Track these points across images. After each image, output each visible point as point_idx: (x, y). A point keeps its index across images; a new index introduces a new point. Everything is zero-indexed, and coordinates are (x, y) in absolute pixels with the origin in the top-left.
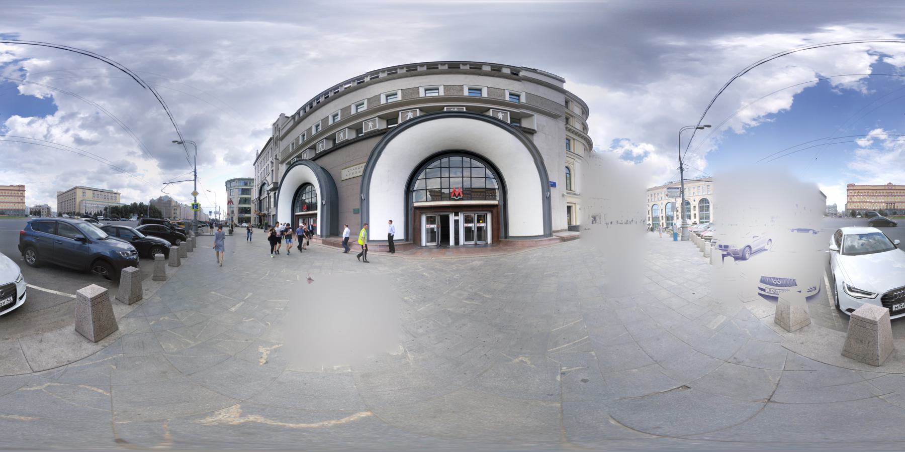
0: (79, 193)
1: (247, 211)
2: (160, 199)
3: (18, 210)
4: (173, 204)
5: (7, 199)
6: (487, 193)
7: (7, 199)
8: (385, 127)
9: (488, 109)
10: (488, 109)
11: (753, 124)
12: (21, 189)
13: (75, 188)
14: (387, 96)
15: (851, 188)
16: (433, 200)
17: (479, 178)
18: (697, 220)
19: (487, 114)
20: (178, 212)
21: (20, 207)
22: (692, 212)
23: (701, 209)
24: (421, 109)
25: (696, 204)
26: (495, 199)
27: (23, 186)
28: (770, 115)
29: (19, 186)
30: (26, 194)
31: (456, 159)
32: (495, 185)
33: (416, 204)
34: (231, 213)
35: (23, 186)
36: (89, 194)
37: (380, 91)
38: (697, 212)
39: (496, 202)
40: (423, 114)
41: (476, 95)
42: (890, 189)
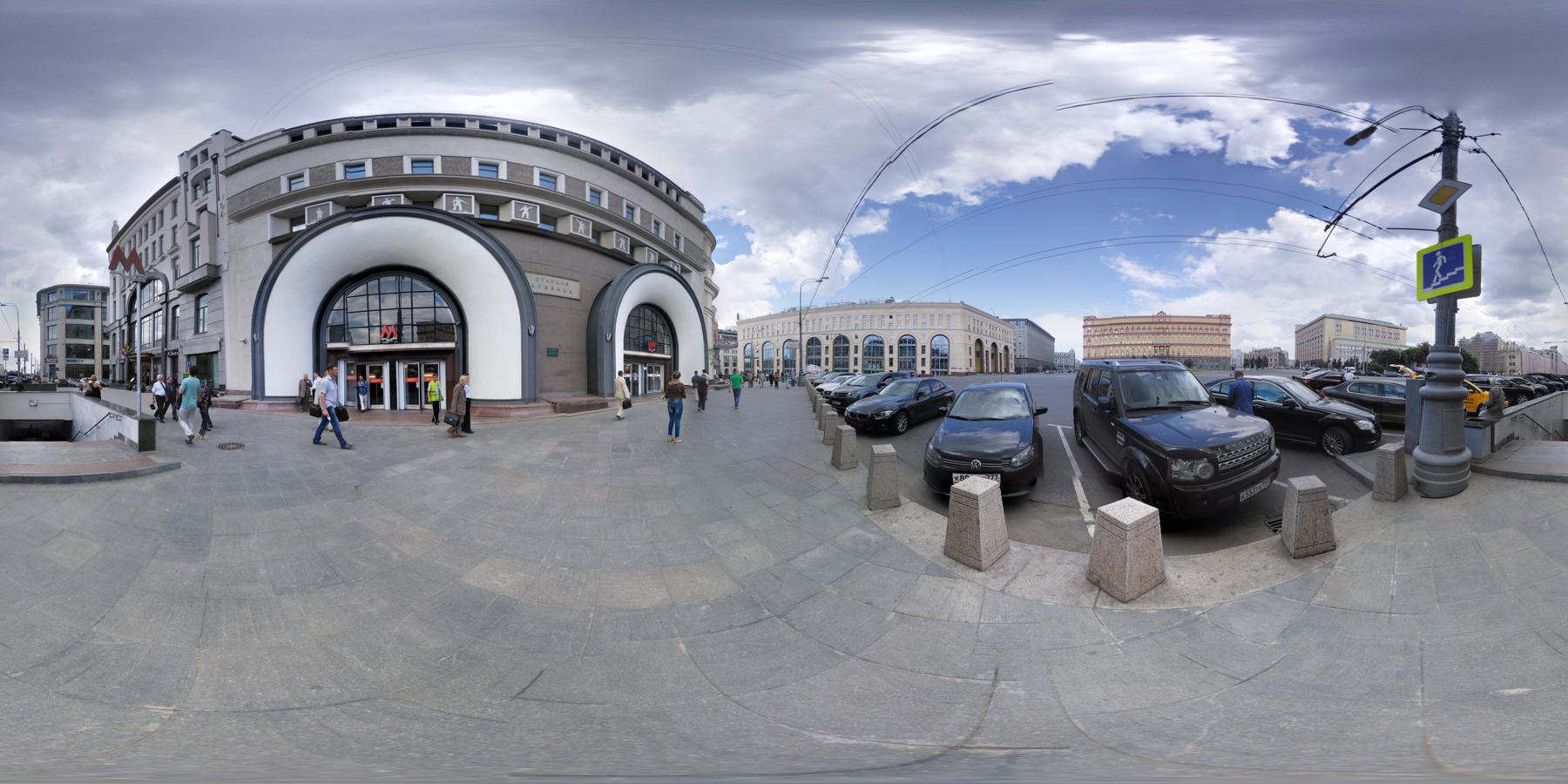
0: (1329, 326)
1: (87, 352)
2: (1478, 338)
3: (1218, 359)
4: (1501, 347)
5: (1198, 339)
6: (430, 330)
7: (1198, 339)
8: (287, 231)
9: (440, 195)
10: (440, 195)
11: (975, 201)
12: (1224, 321)
13: (1323, 318)
14: (290, 179)
15: (1090, 322)
16: (421, 341)
17: (424, 306)
18: (830, 367)
19: (436, 206)
20: (1517, 361)
21: (1221, 353)
22: (823, 356)
23: (836, 351)
24: (336, 201)
25: (830, 343)
26: (452, 340)
27: (1228, 317)
28: (1013, 186)
29: (1220, 317)
30: (1233, 330)
31: (389, 281)
32: (447, 315)
33: (330, 346)
34: (48, 357)
35: (1228, 317)
36: (1348, 328)
37: (505, 155)
38: (830, 356)
39: (451, 345)
40: (342, 209)
41: (422, 171)
42: (1162, 322)
